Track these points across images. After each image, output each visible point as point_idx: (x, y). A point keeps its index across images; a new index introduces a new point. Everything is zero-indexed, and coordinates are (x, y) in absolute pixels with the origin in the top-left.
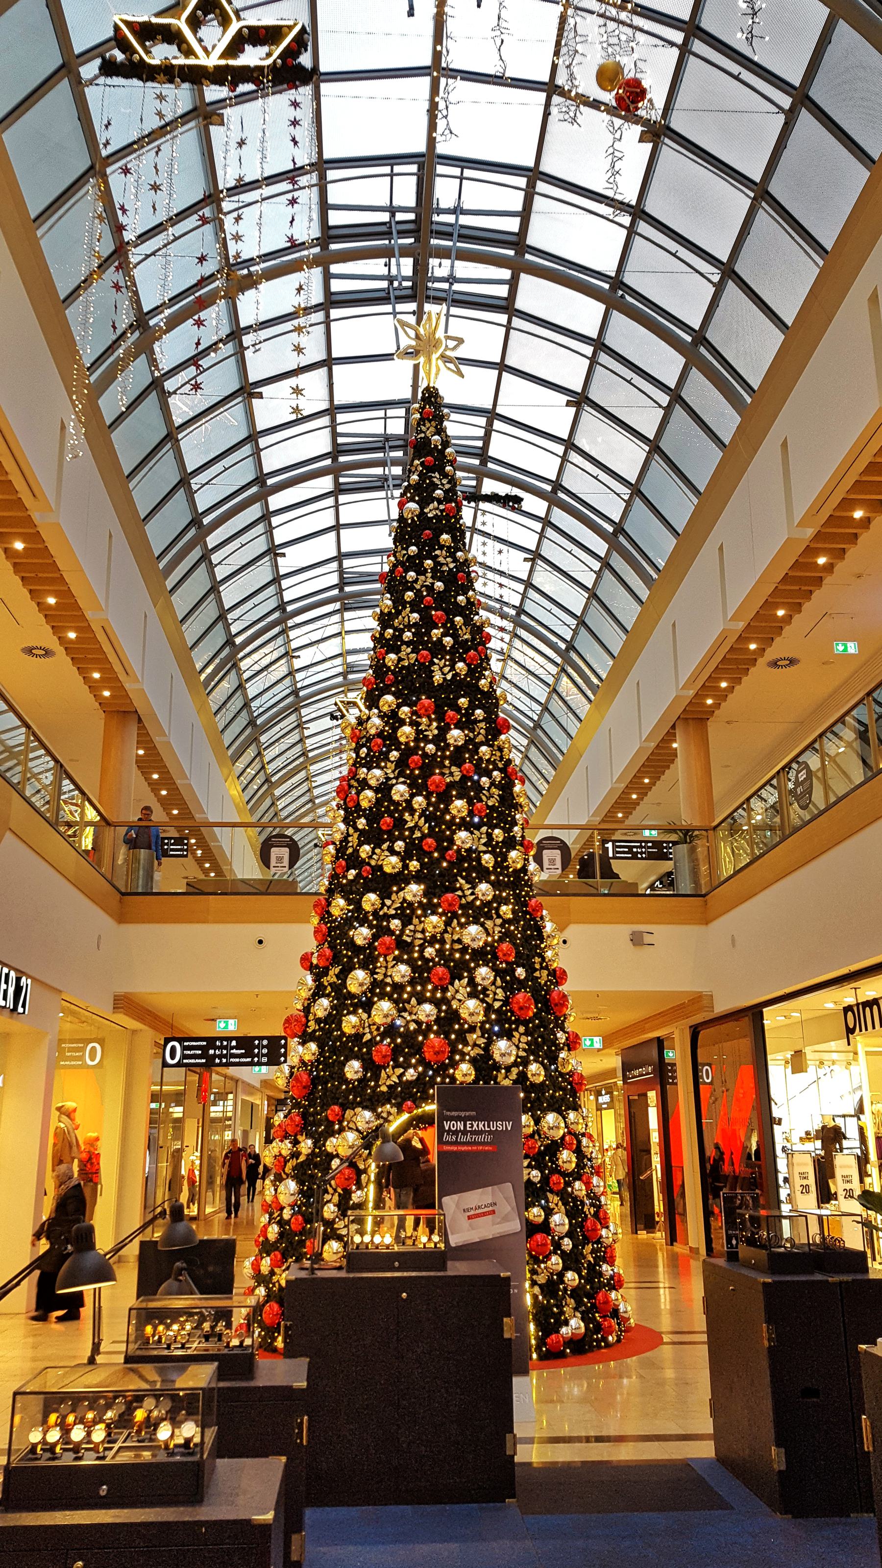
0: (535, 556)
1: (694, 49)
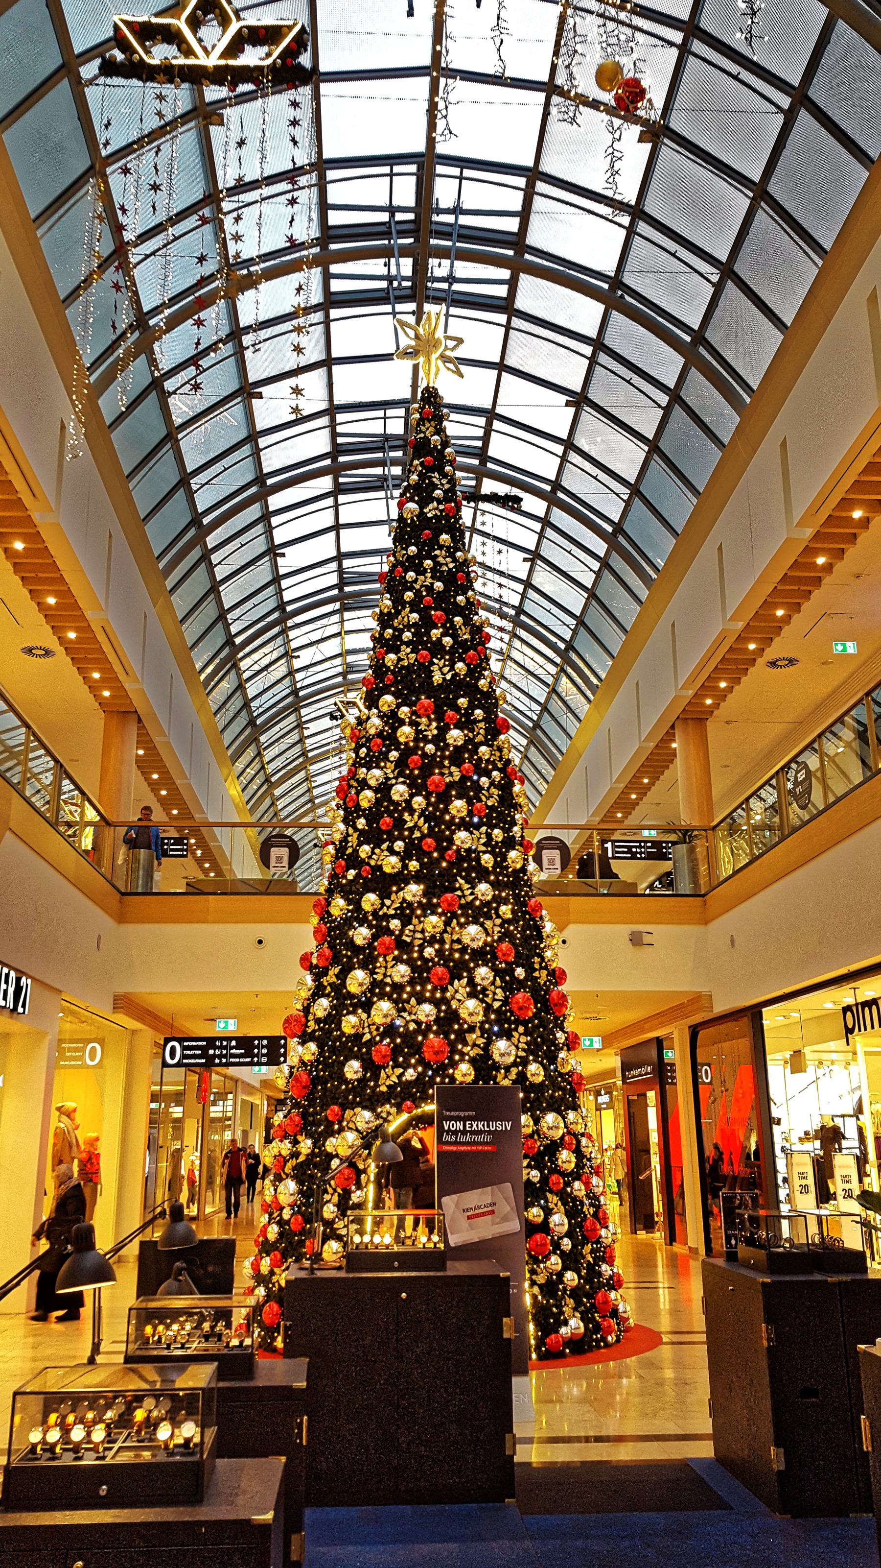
0: (535, 556)
1: (693, 49)
